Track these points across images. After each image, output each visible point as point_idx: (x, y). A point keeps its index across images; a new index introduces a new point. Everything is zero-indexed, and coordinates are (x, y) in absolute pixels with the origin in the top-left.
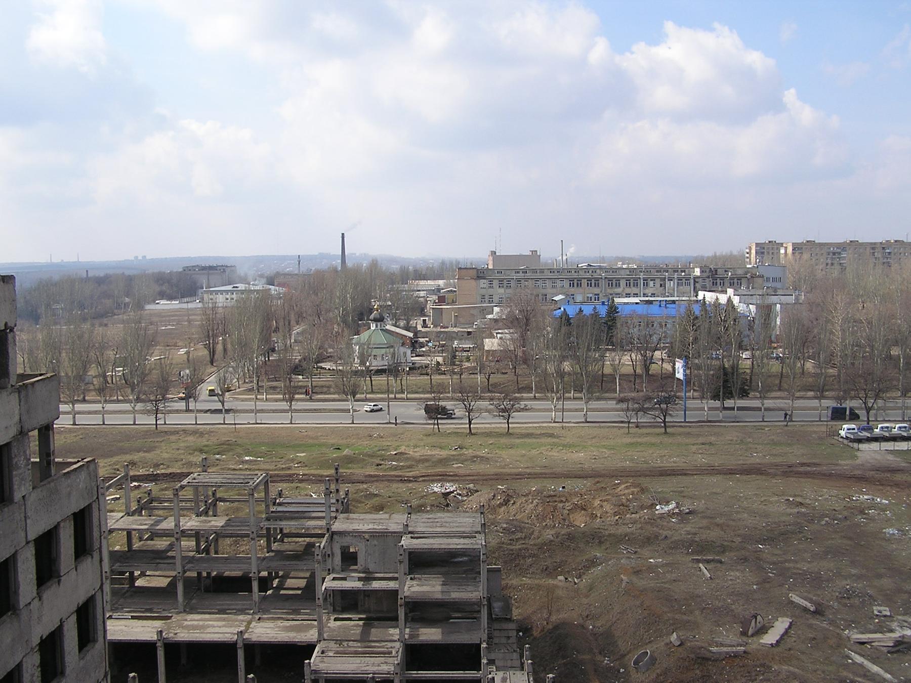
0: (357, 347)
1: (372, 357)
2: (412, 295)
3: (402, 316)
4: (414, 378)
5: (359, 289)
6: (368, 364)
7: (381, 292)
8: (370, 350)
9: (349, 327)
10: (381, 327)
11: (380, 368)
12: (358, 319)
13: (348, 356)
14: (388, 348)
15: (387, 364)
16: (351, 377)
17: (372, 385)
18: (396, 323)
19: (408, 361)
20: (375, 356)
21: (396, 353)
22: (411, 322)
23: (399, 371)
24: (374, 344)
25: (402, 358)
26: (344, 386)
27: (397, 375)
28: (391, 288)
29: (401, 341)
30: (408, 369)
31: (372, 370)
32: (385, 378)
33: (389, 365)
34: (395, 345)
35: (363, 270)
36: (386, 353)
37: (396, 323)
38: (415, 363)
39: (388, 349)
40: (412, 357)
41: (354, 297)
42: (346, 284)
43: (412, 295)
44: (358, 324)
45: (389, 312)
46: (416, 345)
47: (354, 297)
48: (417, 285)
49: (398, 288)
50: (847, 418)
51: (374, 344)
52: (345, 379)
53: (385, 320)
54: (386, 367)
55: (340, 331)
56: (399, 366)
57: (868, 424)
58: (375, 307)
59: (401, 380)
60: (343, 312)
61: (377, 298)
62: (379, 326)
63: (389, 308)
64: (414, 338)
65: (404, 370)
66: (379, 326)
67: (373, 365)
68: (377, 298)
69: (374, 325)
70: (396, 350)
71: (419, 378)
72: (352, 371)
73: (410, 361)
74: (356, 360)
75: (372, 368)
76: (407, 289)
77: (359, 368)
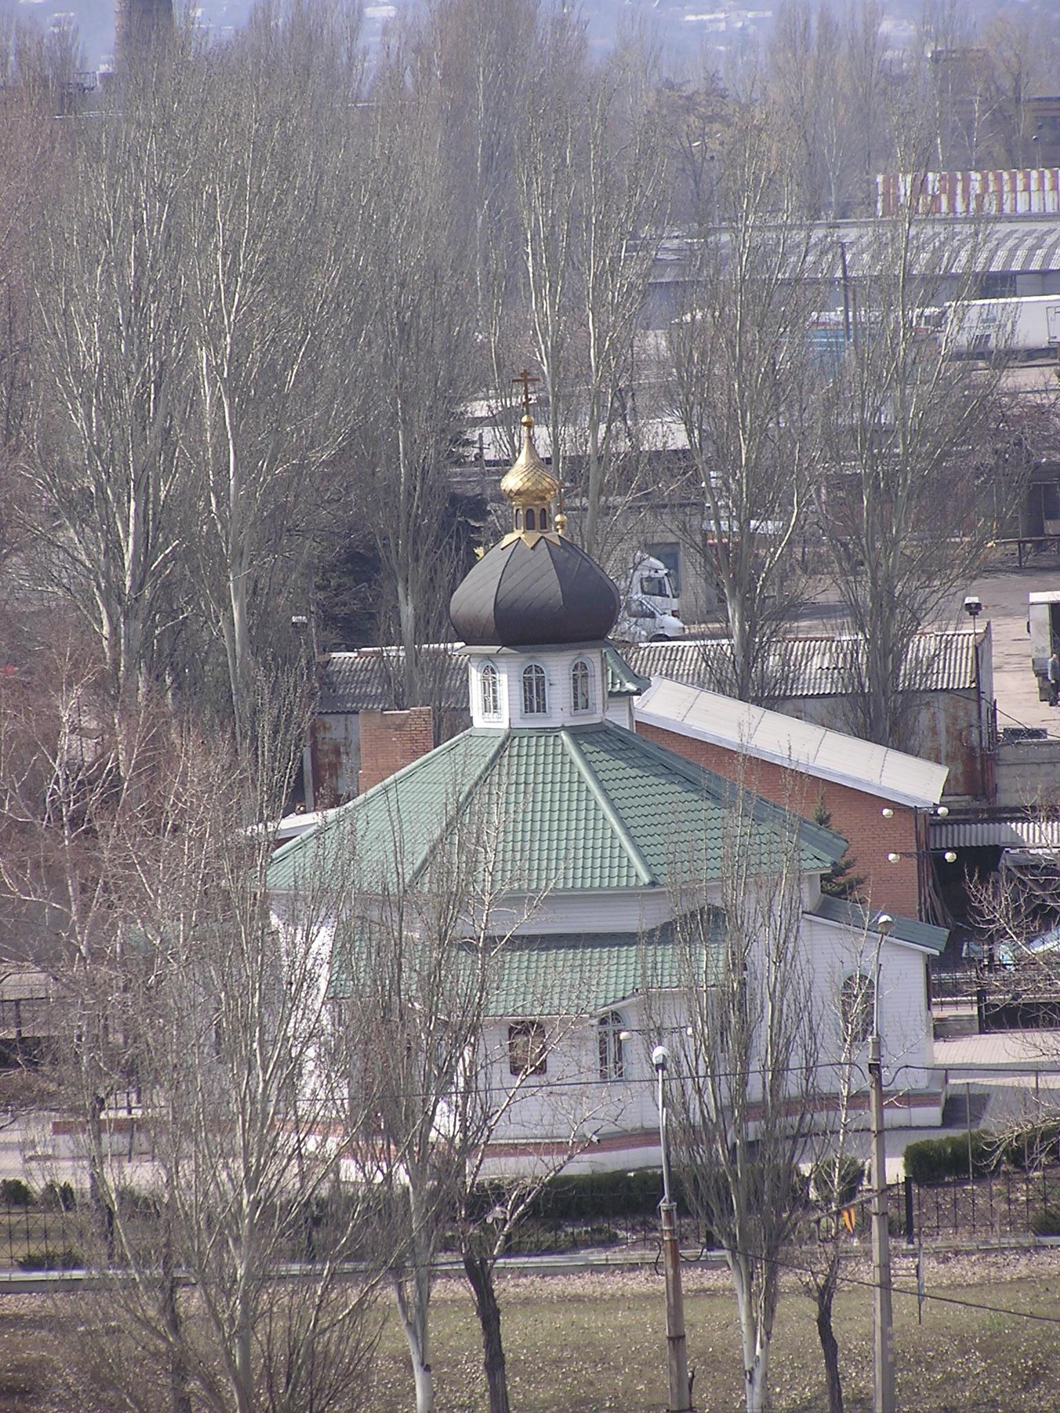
0: (323, 940)
1: (495, 1044)
2: (923, 340)
3: (810, 568)
4: (966, 1270)
5: (324, 280)
6: (445, 1122)
7: (571, 307)
8: (464, 969)
9: (227, 713)
10: (580, 701)
11: (581, 1166)
12: (328, 619)
13: (224, 1048)
14: (665, 934)
15: (660, 1118)
16: (260, 1279)
17: (495, 1362)
18: (750, 653)
19: (904, 1083)
20: (520, 1029)
21: (761, 991)
22: (924, 644)
23: (800, 1201)
24: (515, 899)
25: (831, 1047)
26: (180, 1371)
27: (778, 1236)
28: (686, 258)
29: (817, 862)
30: (896, 1169)
31: (497, 1193)
32: (638, 1283)
33: (691, 1135)
34: (749, 904)
35: (373, 62)
36: (648, 997)
37: (750, 653)
38: (980, 1101)
39: (667, 956)
40: (942, 1031)
41: (272, 373)
42: (174, 239)
43: (923, 340)
44: (326, 678)
45: (665, 530)
46: (982, 896)
47: (272, 373)
48: (979, 219)
49: (761, 256)
50: (937, 1013)
51: (515, 899)
52: (191, 1301)
53: (625, 626)
54: (654, 1155)
55: (123, 759)
56: (801, 1136)
57: (130, 1113)
58: (512, 481)
59: (825, 1295)
60: (146, 549)
61: (526, 378)
62: (559, 694)
63: (670, 488)
64: (959, 817)
65: (854, 1177)
66: (559, 694)
67: (504, 1131)
68: (526, 378)
69: (507, 685)
70: (760, 956)
71: (1022, 1267)
72: (267, 1210)
73: (919, 1081)
74: (310, 1083)
75: (494, 1169)
76: (862, 264)
77: (349, 1170)
